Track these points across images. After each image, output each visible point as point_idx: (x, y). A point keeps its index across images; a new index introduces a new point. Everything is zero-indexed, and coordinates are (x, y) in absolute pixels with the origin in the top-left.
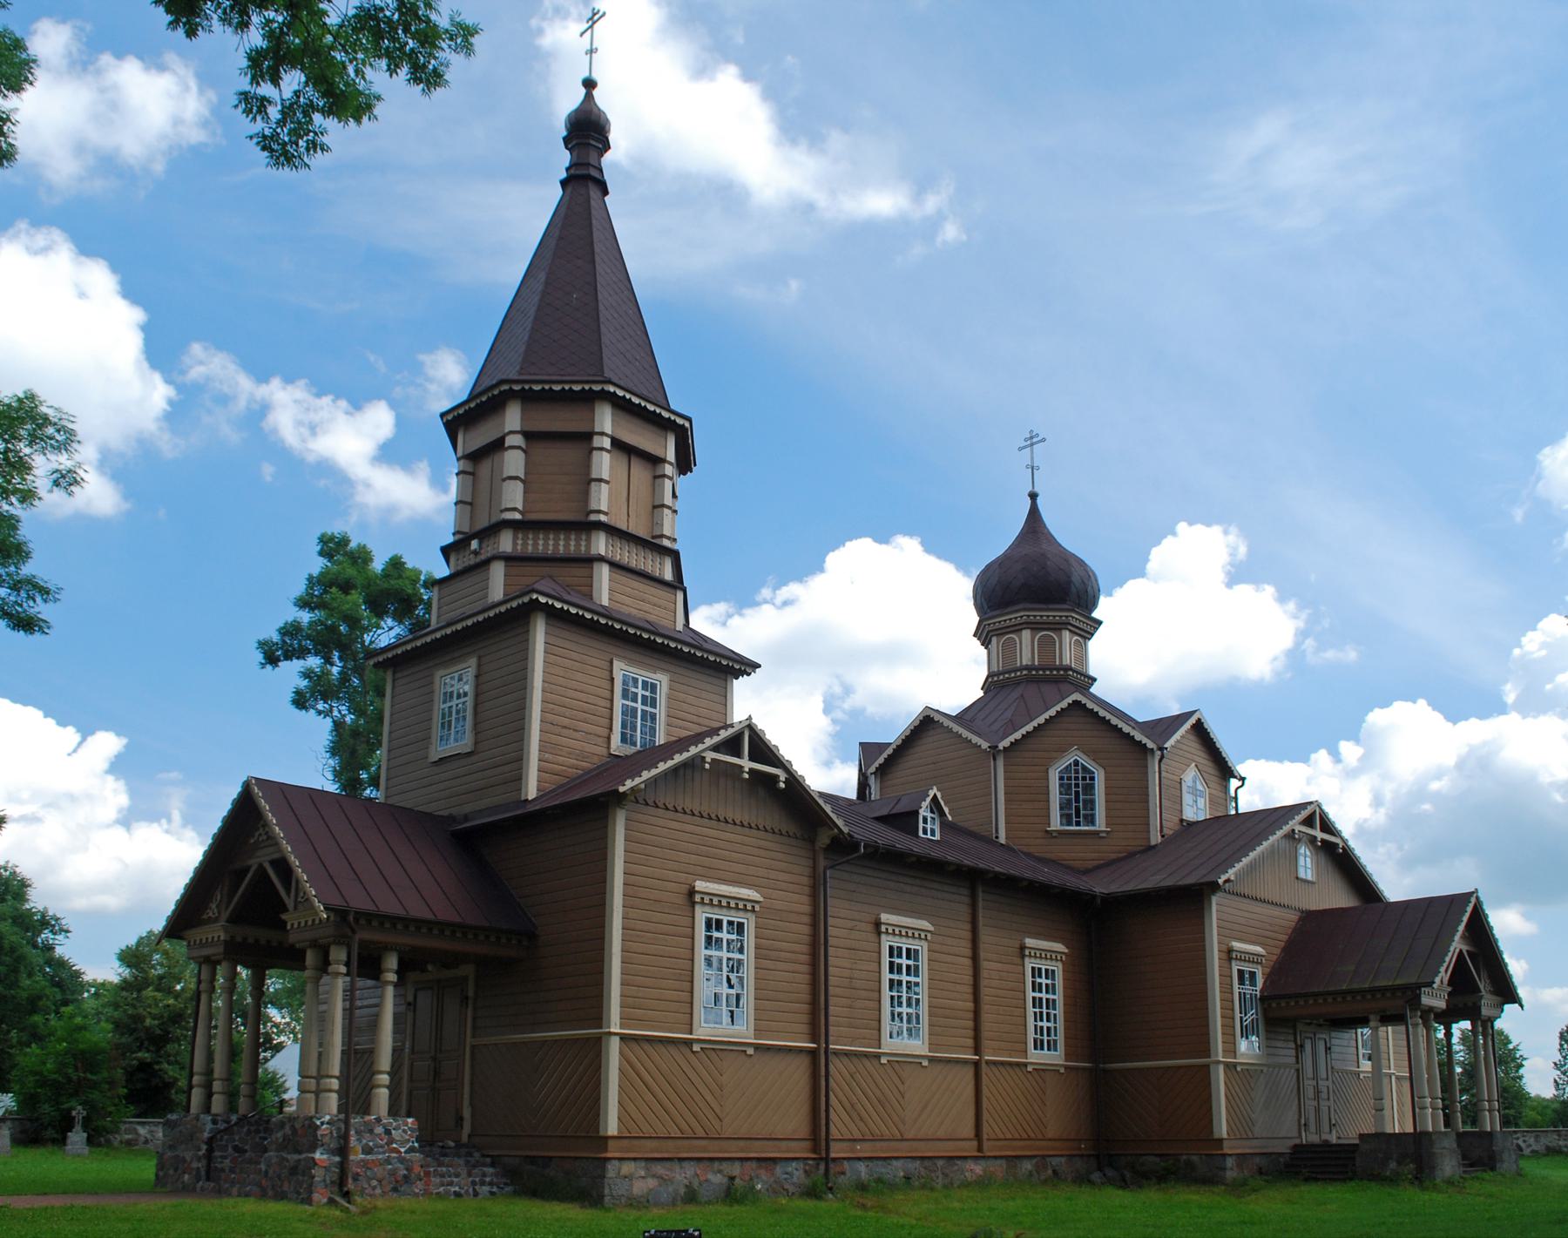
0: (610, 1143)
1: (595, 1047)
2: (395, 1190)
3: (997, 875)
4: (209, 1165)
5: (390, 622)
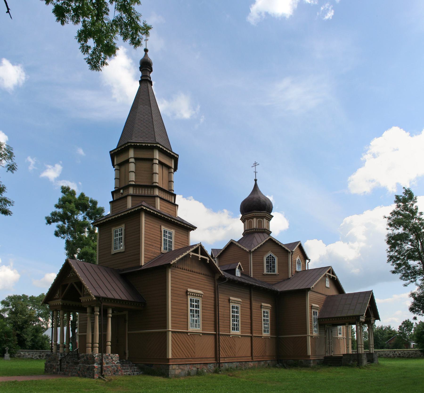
0: (170, 360)
1: (165, 334)
2: (114, 374)
3: (259, 287)
4: (61, 367)
5: (81, 213)
